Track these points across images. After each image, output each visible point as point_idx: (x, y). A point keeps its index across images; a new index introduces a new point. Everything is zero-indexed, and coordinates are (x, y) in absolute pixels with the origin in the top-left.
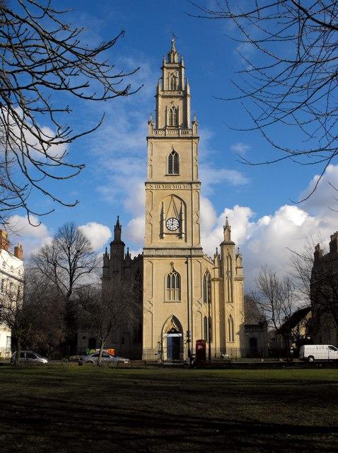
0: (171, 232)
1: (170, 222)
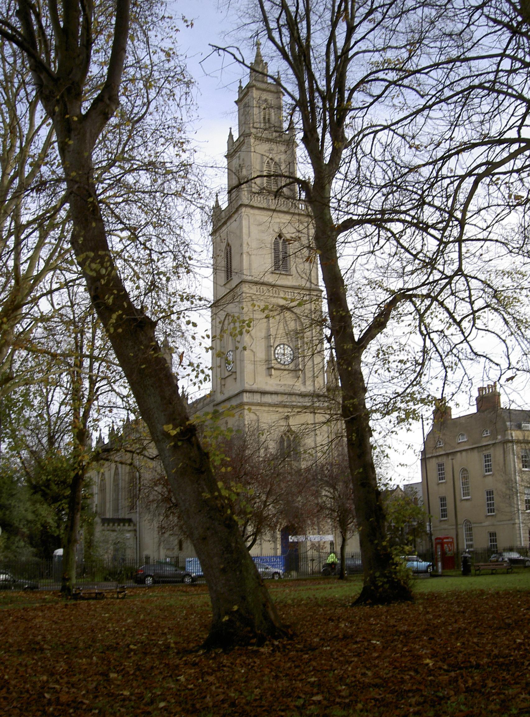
0: (283, 367)
1: (279, 350)
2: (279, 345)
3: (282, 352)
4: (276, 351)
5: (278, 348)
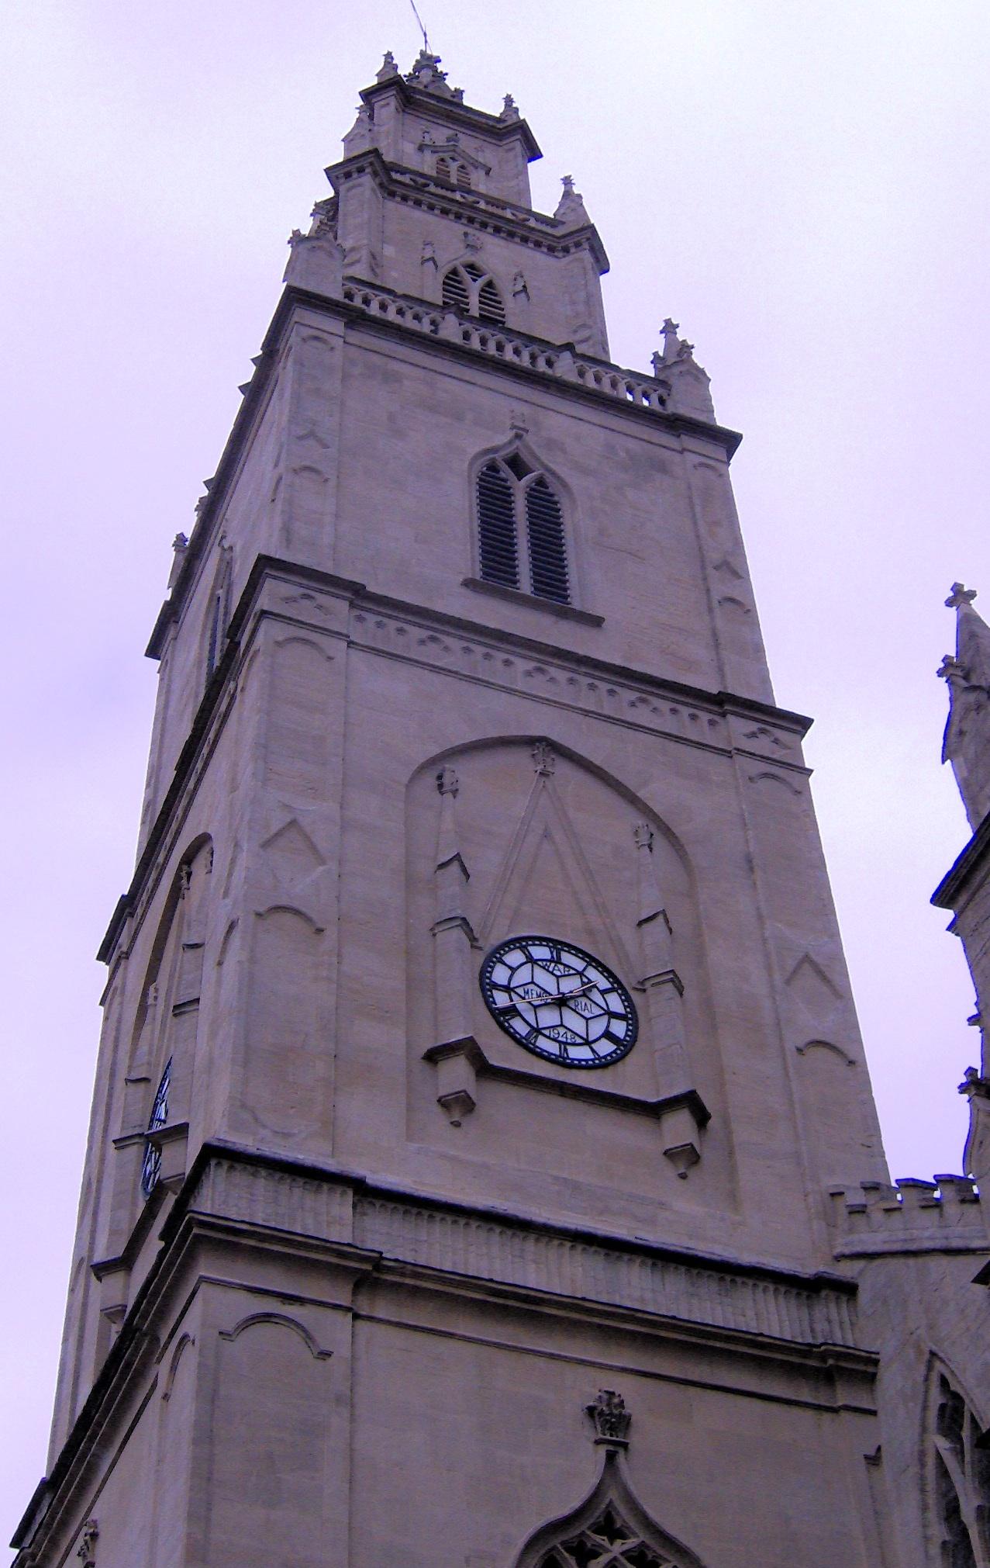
2: (520, 943)
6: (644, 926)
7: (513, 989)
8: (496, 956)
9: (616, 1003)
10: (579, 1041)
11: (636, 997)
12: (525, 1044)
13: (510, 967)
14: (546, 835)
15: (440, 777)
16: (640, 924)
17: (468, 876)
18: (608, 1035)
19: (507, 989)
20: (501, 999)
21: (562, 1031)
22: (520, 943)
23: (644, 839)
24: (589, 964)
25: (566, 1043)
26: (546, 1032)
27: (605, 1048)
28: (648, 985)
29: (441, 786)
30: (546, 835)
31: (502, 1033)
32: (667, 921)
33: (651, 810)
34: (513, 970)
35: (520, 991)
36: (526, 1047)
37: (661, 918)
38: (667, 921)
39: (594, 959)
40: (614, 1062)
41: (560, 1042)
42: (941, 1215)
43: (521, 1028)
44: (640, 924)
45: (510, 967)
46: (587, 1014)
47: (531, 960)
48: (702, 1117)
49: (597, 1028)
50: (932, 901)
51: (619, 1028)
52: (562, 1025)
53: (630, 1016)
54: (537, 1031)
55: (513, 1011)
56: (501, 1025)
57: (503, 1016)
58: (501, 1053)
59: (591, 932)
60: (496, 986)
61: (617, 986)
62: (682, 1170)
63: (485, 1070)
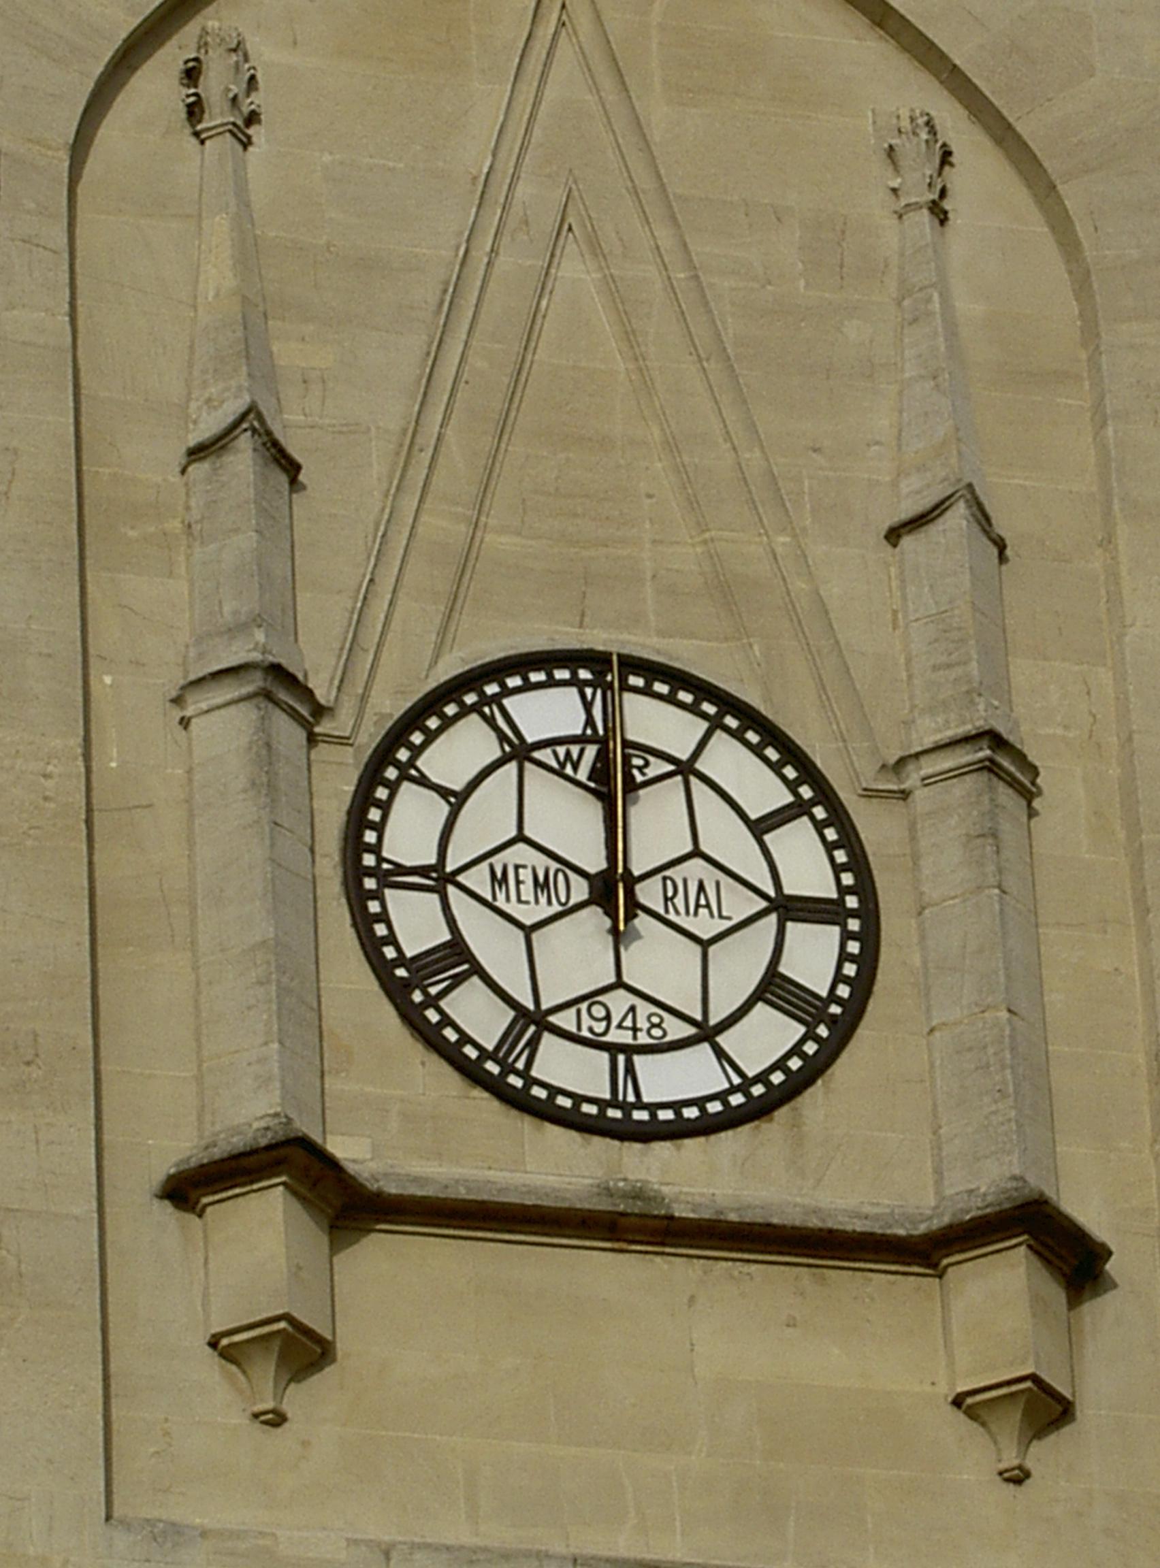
0: (561, 1167)
2: (474, 689)
3: (567, 822)
4: (410, 830)
5: (460, 750)
6: (907, 542)
7: (451, 878)
8: (389, 760)
9: (805, 864)
10: (677, 1030)
11: (875, 827)
12: (498, 1079)
13: (444, 792)
14: (570, 229)
15: (192, 74)
16: (894, 535)
17: (291, 468)
18: (774, 988)
19: (439, 878)
20: (415, 923)
21: (619, 1002)
22: (474, 689)
23: (916, 181)
24: (716, 724)
25: (630, 1050)
26: (566, 1020)
27: (766, 1039)
28: (912, 778)
29: (194, 111)
30: (570, 229)
31: (416, 1050)
32: (983, 518)
33: (943, 56)
34: (457, 799)
35: (478, 879)
36: (497, 1089)
37: (958, 517)
38: (983, 518)
39: (729, 704)
40: (797, 1085)
41: (613, 1049)
42: (941, 1286)
43: (476, 1015)
44: (894, 535)
45: (444, 792)
46: (705, 926)
47: (519, 751)
48: (1077, 1263)
49: (738, 970)
50: (1110, 1253)
51: (814, 957)
52: (619, 984)
53: (856, 907)
54: (532, 1022)
55: (455, 956)
56: (411, 1017)
57: (413, 986)
58: (398, 1119)
59: (725, 589)
60: (394, 876)
61: (814, 795)
62: (1010, 1459)
63: (348, 1206)
